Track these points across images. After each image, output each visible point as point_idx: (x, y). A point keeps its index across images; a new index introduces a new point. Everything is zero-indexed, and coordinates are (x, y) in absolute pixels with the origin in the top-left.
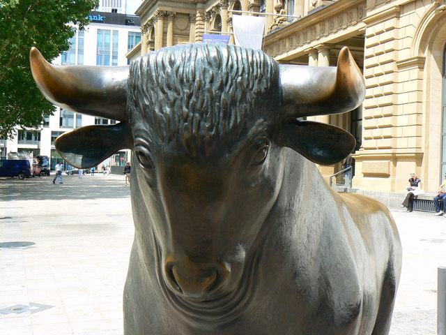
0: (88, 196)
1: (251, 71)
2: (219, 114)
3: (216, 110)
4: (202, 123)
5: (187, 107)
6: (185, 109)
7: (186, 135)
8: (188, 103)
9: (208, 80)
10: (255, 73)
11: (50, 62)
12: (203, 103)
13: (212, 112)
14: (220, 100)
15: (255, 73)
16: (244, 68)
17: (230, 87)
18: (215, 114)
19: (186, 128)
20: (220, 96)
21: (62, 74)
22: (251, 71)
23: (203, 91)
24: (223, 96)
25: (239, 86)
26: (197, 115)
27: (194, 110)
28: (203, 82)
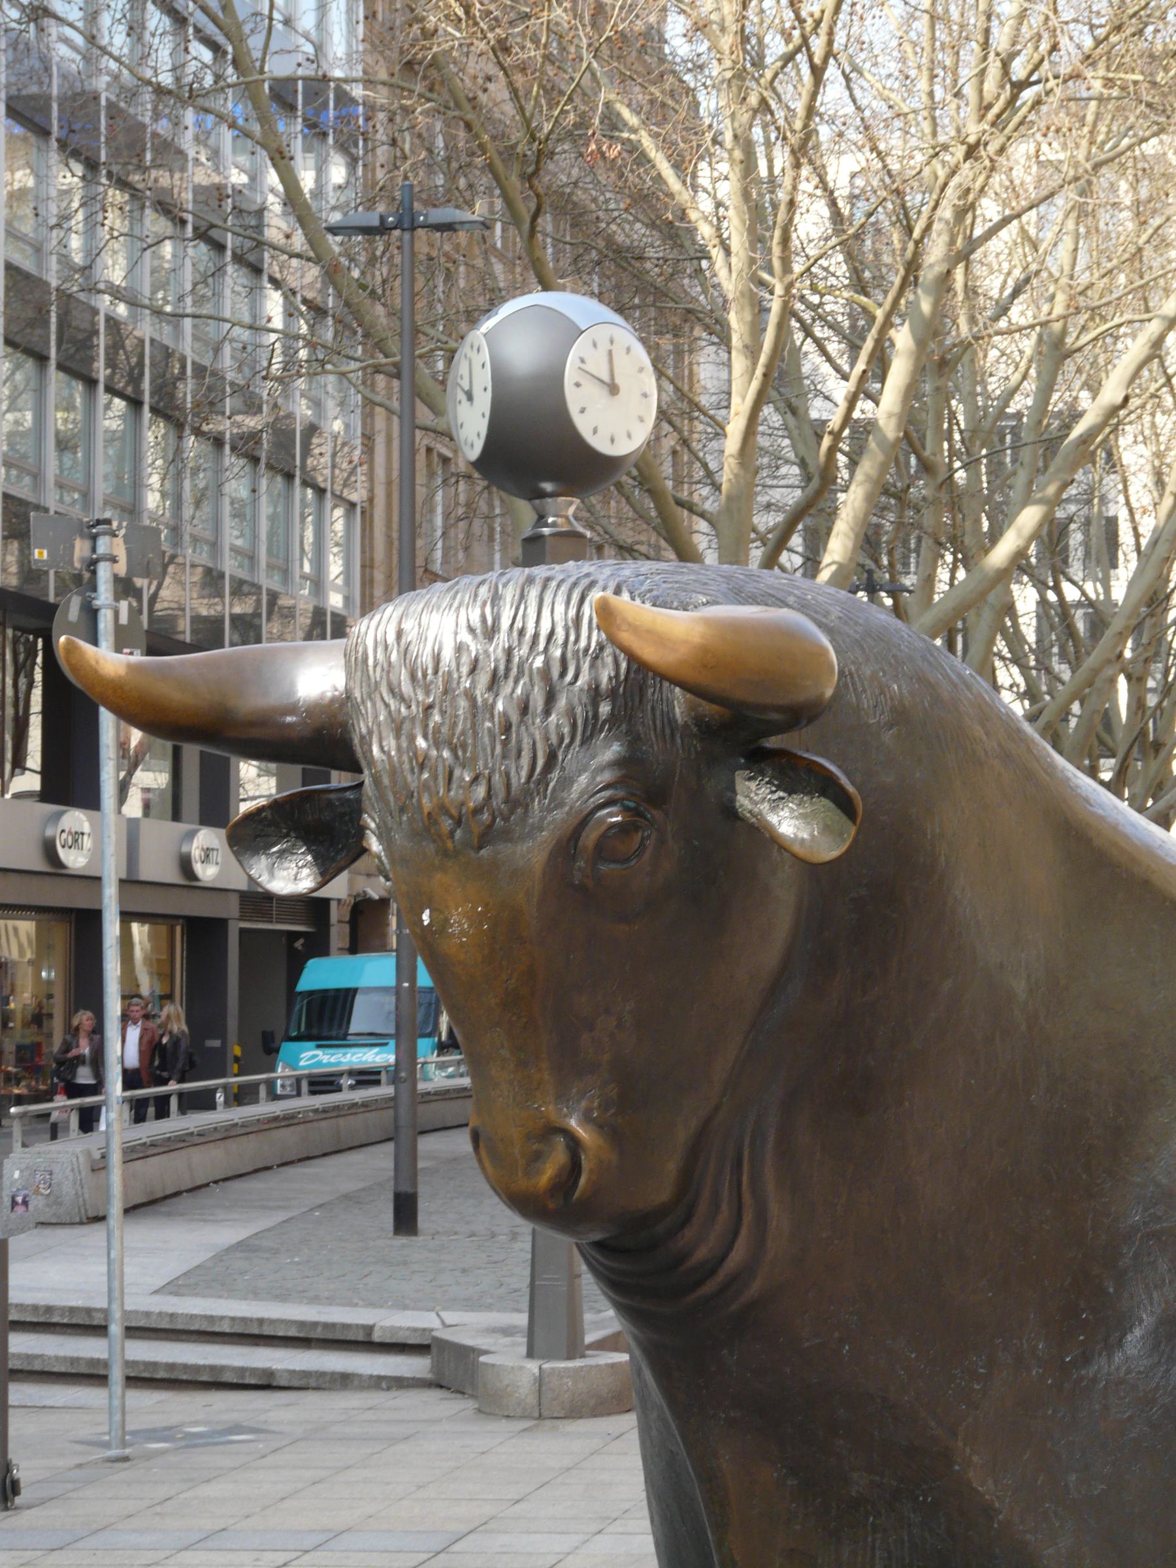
0: (162, 1150)
1: (572, 638)
2: (493, 749)
3: (486, 740)
4: (457, 772)
5: (425, 737)
6: (421, 743)
7: (427, 803)
8: (427, 726)
9: (465, 670)
10: (583, 643)
11: (348, 692)
12: (455, 724)
13: (475, 746)
14: (492, 716)
15: (583, 643)
16: (552, 634)
17: (516, 682)
18: (484, 750)
19: (425, 786)
20: (493, 706)
21: (120, 677)
22: (572, 638)
23: (454, 698)
24: (500, 706)
25: (537, 679)
26: (446, 754)
27: (437, 744)
28: (455, 676)
